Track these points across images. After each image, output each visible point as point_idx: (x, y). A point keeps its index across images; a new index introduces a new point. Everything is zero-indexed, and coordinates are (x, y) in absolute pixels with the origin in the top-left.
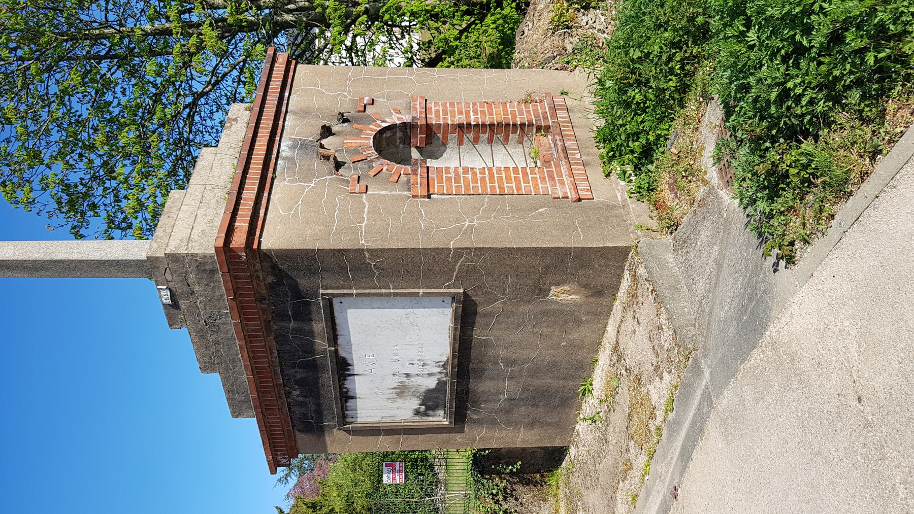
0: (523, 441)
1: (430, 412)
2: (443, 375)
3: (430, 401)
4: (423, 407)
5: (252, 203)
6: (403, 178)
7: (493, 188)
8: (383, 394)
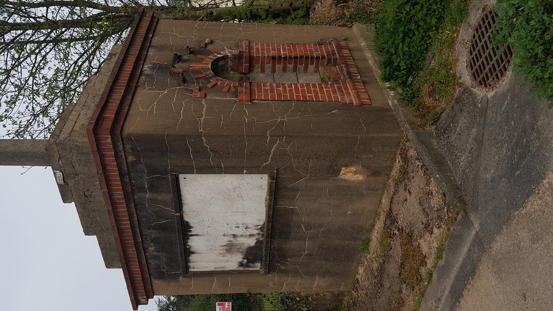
0: (318, 287)
1: (251, 264)
2: (260, 236)
3: (251, 255)
4: (246, 260)
5: (119, 102)
6: (233, 89)
7: (298, 97)
8: (216, 250)
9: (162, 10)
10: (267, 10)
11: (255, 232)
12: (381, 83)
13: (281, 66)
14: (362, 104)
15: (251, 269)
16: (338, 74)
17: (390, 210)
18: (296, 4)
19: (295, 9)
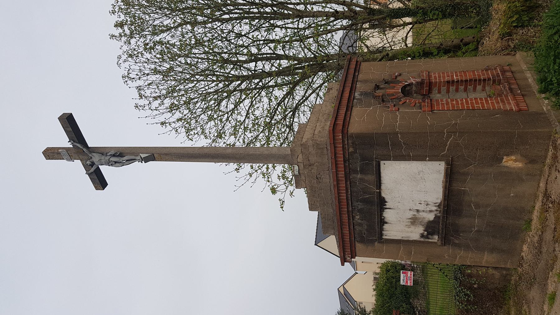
1: (430, 236)
3: (431, 228)
8: (403, 222)
9: (344, 57)
10: (438, 48)
11: (434, 208)
12: (538, 95)
13: (454, 88)
14: (520, 110)
15: (430, 240)
16: (501, 90)
17: (546, 189)
18: (466, 40)
19: (466, 44)
